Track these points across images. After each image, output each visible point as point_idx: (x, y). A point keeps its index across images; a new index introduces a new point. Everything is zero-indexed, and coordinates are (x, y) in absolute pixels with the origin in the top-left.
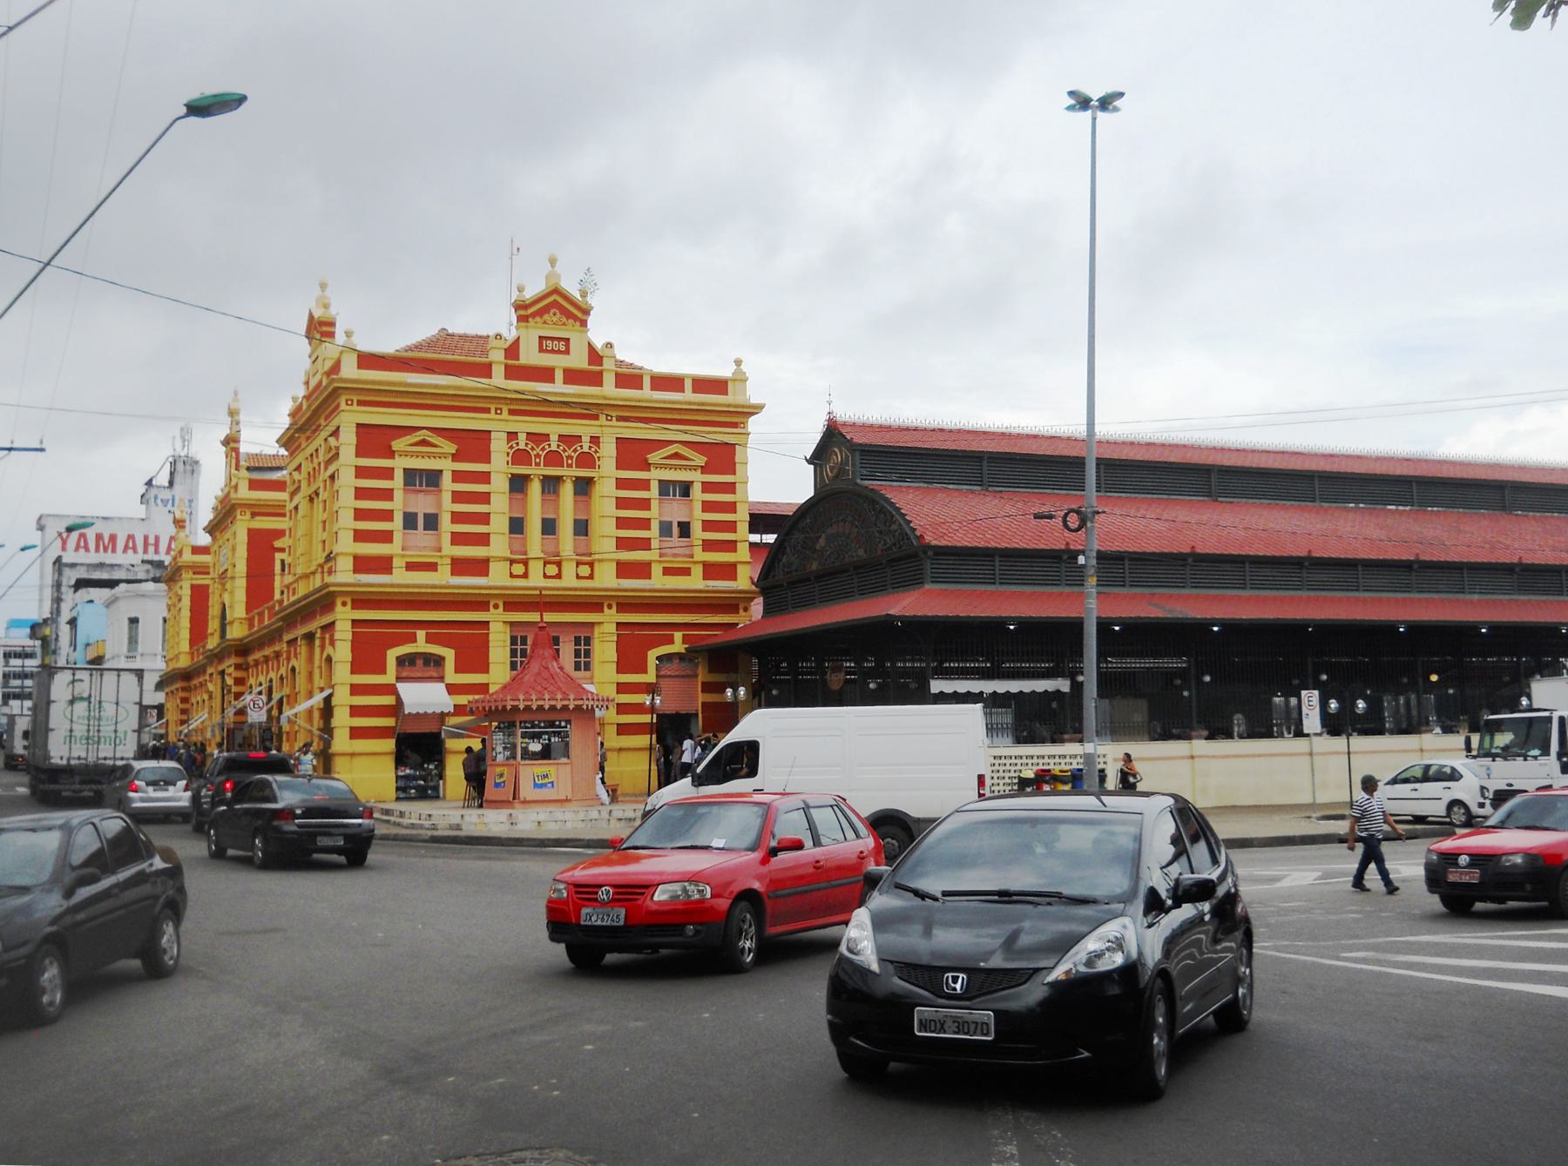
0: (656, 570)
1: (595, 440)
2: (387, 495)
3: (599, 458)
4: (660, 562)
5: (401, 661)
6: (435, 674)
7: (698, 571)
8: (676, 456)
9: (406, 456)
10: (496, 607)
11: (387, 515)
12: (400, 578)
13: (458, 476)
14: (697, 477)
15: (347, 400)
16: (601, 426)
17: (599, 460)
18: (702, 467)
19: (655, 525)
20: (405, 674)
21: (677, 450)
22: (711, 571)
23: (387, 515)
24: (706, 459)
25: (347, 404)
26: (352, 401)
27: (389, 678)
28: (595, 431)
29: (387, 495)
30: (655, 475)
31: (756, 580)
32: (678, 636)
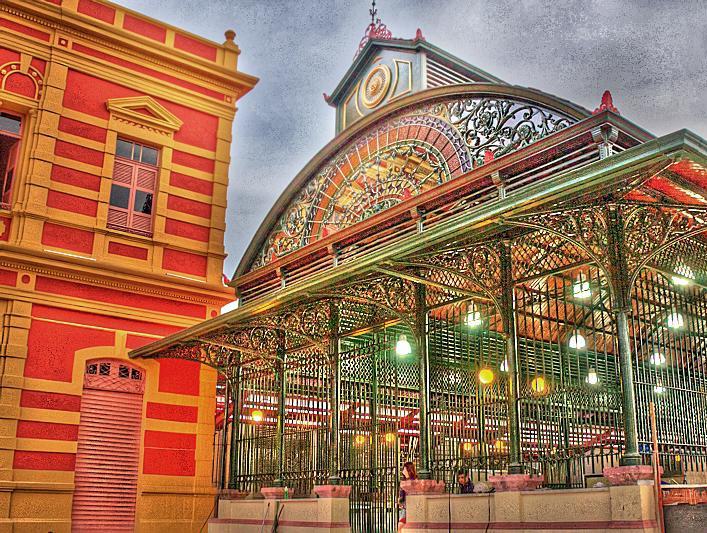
0: (101, 242)
1: (40, 63)
2: (97, 158)
3: (41, 86)
4: (107, 234)
5: (91, 367)
6: (133, 389)
7: (156, 254)
8: (145, 110)
9: (142, 126)
10: (26, 279)
11: (94, 183)
12: (100, 254)
13: (179, 157)
14: (169, 142)
15: (60, 39)
16: (51, 48)
17: (40, 89)
18: (176, 132)
19: (106, 187)
20: (93, 385)
21: (146, 104)
22: (172, 256)
23: (94, 183)
24: (181, 123)
25: (60, 43)
26: (67, 41)
27: (74, 387)
28: (43, 53)
29: (97, 158)
30: (115, 125)
31: (230, 279)
32: (121, 335)
